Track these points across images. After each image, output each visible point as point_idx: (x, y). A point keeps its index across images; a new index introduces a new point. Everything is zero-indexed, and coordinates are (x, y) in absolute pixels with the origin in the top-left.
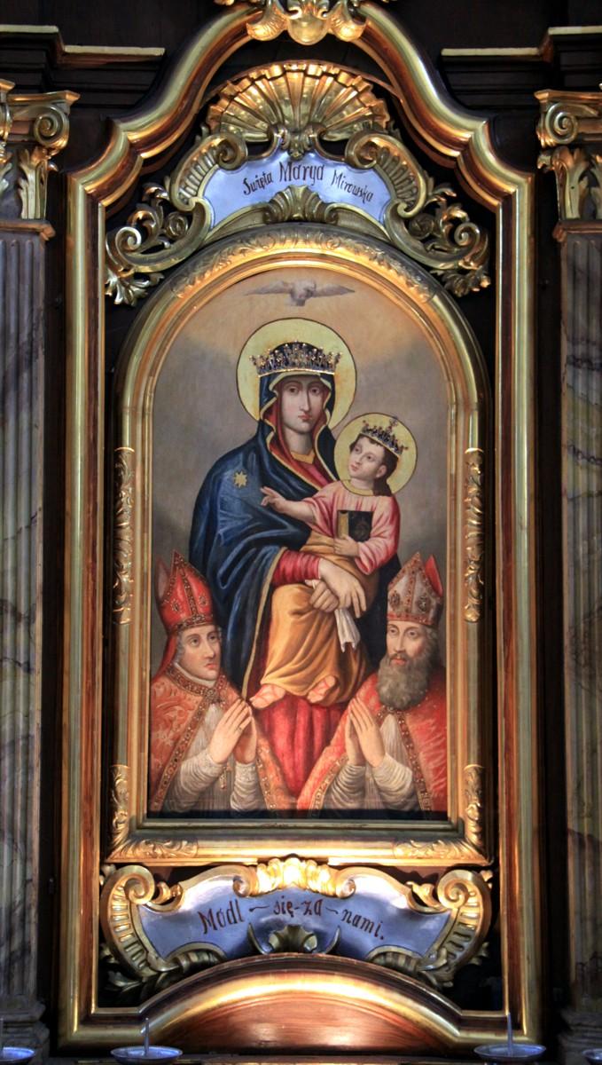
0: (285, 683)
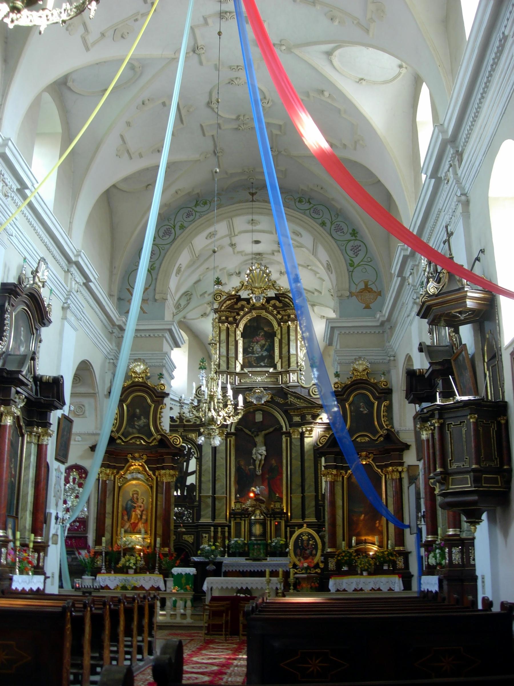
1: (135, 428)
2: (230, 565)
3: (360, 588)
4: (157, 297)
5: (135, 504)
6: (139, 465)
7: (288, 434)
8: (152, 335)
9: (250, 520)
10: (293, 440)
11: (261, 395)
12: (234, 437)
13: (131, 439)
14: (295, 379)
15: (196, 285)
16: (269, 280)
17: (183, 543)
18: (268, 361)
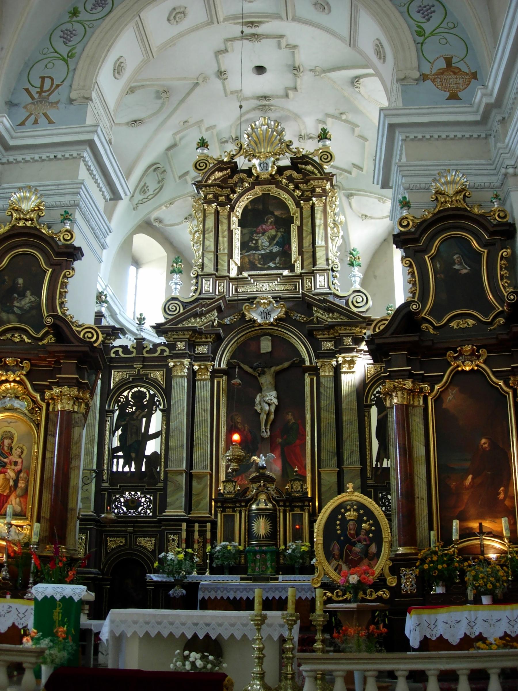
1: (14, 312)
2: (213, 589)
3: (477, 634)
5: (6, 457)
6: (14, 381)
7: (315, 371)
8: (59, 156)
9: (249, 510)
10: (322, 380)
11: (269, 308)
12: (225, 377)
15: (170, 153)
16: (281, 141)
17: (138, 551)
18: (280, 260)
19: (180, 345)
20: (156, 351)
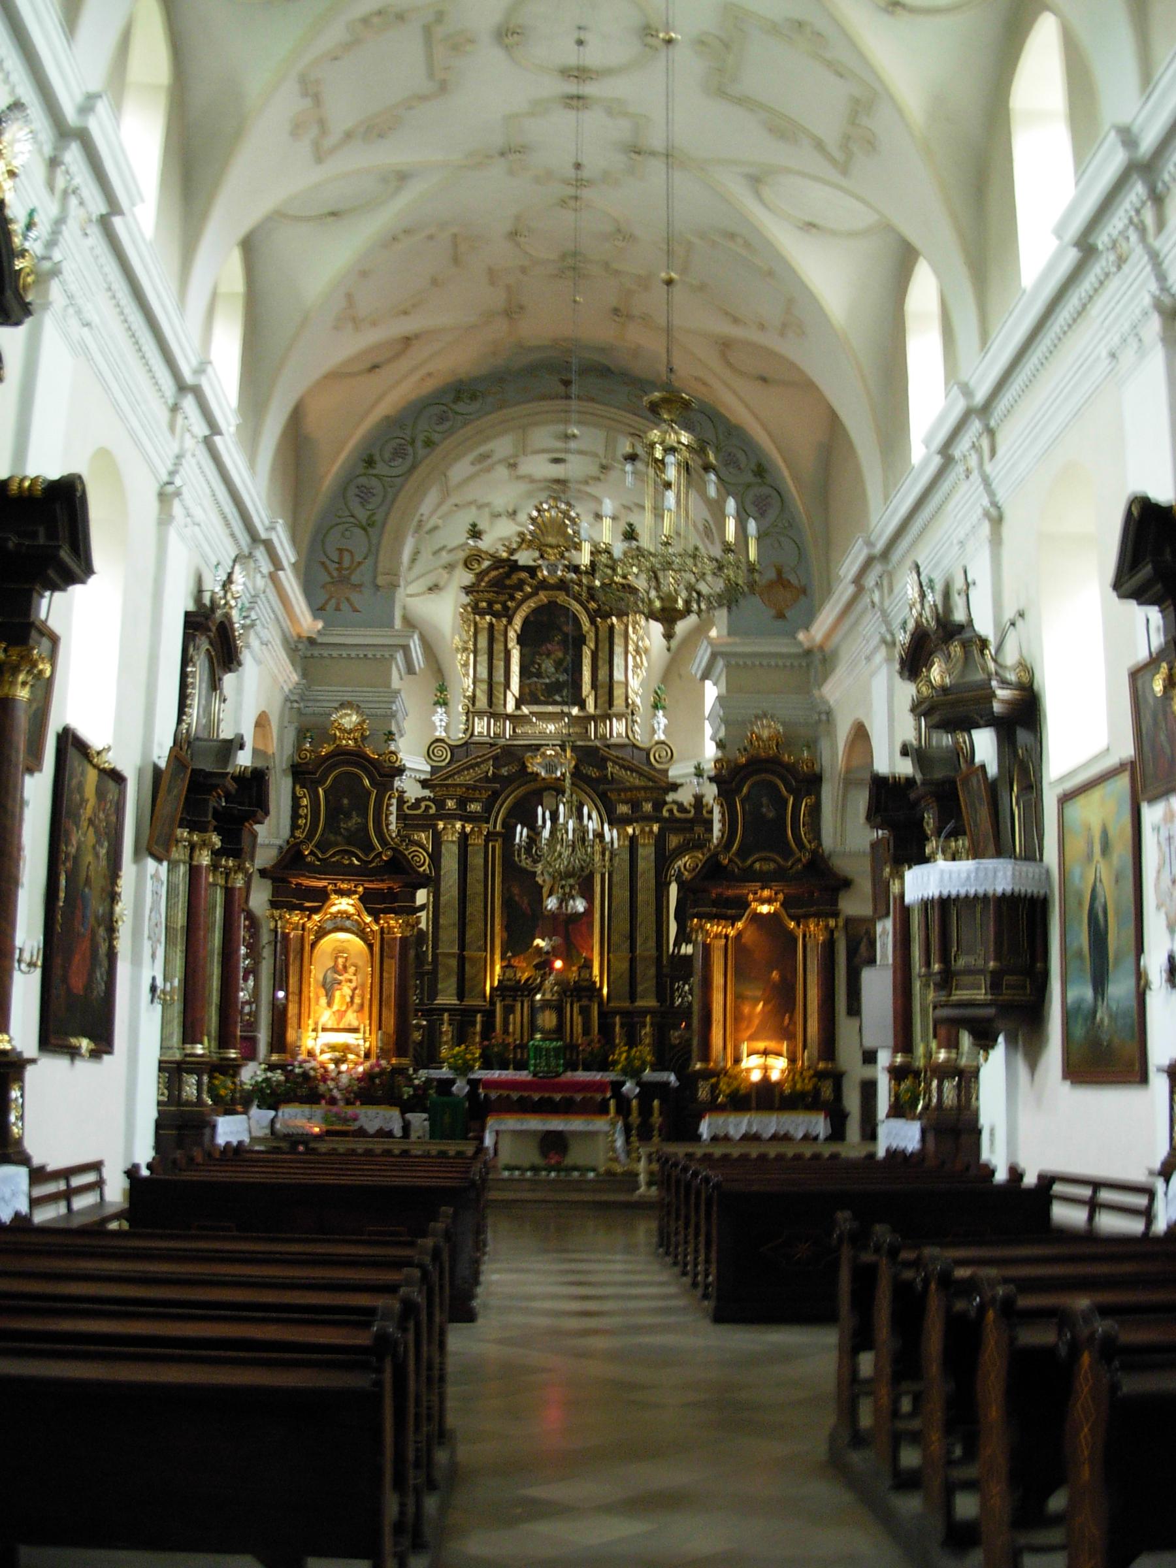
0: (473, 464)
1: (341, 834)
4: (381, 580)
9: (533, 1001)
12: (500, 840)
13: (333, 856)
14: (622, 730)
19: (450, 804)
20: (419, 807)
